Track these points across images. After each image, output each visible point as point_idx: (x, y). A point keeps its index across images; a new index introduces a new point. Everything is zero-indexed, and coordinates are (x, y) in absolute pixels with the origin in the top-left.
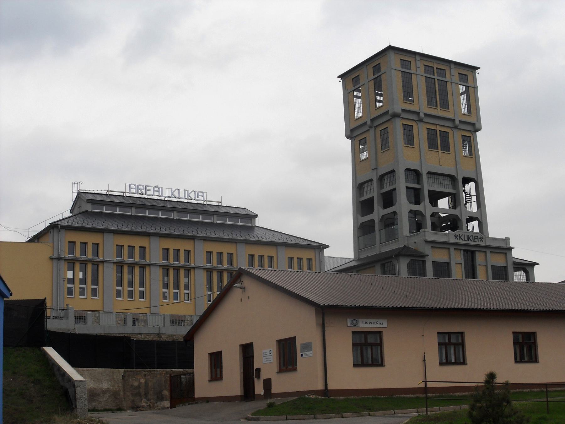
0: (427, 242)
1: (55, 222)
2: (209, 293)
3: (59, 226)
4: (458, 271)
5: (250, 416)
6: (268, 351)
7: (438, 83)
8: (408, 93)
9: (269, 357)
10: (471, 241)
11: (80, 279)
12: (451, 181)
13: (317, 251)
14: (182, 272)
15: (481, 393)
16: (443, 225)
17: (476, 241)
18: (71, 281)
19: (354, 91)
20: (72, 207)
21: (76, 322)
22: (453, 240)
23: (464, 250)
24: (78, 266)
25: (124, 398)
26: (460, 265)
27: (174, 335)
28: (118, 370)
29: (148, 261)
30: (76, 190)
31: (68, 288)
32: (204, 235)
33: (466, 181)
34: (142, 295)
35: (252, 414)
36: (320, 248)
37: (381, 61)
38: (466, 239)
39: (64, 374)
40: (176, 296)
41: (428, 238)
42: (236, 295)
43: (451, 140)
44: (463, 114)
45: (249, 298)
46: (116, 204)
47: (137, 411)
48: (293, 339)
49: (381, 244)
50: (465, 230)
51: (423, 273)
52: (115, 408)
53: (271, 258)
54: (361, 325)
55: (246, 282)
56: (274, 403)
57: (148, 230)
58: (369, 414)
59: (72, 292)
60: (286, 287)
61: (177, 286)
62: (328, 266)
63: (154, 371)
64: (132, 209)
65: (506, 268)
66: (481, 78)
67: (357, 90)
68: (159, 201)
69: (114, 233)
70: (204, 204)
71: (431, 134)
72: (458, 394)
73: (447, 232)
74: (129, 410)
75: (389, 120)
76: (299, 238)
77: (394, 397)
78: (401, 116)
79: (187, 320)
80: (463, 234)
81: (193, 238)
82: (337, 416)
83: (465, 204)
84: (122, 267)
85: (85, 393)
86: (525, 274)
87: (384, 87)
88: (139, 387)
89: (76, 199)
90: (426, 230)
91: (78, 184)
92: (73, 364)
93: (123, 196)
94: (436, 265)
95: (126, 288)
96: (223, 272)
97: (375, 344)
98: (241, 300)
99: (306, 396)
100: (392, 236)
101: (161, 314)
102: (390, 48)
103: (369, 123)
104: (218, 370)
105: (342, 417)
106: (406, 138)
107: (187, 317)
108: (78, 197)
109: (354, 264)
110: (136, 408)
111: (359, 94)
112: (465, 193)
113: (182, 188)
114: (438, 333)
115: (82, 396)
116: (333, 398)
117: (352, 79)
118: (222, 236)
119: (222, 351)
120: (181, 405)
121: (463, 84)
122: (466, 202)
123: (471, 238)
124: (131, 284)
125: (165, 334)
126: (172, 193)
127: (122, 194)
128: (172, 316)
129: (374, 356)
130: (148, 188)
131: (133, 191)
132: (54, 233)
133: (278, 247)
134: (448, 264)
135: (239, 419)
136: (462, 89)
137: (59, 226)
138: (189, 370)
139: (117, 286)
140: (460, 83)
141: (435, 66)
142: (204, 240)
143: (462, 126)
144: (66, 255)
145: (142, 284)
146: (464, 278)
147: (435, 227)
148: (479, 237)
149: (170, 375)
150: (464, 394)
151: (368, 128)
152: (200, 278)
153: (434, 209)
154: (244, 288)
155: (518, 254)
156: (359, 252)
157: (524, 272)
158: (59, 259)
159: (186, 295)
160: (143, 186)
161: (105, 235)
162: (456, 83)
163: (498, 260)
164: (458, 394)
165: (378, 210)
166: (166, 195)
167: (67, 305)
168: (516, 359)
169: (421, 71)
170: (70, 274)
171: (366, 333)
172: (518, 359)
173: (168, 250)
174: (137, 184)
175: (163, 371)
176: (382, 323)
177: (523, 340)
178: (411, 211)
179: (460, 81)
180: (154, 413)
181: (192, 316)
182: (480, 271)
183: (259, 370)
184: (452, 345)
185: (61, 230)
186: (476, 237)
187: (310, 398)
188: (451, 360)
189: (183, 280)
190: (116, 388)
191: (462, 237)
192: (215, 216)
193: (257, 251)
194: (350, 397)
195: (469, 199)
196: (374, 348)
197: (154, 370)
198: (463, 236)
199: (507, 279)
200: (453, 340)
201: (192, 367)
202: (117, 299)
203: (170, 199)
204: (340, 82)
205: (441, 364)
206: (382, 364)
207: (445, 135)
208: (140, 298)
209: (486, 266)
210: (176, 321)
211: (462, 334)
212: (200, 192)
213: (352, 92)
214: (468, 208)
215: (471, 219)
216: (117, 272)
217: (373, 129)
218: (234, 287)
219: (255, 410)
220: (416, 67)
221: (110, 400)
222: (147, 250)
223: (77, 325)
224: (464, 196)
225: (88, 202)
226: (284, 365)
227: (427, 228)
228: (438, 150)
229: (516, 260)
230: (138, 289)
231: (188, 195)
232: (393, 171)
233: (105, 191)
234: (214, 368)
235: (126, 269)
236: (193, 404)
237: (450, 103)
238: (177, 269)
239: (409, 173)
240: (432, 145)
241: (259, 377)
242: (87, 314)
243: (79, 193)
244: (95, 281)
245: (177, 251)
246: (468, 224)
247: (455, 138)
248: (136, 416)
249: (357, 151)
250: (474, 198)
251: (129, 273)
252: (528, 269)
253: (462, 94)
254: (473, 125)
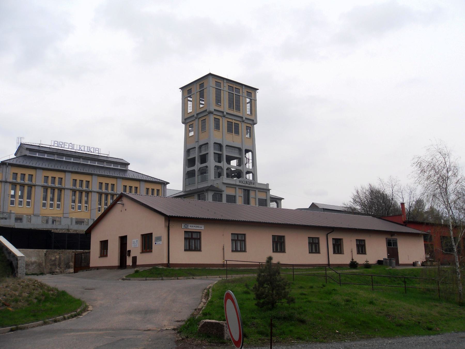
0: (224, 183)
1: (4, 161)
2: (100, 206)
3: (7, 164)
4: (240, 200)
5: (125, 278)
6: (135, 240)
7: (235, 96)
8: (218, 100)
9: (136, 244)
10: (248, 184)
11: (19, 195)
12: (239, 151)
13: (163, 185)
14: (84, 194)
15: (264, 268)
16: (233, 175)
17: (250, 185)
18: (13, 196)
19: (188, 97)
20: (16, 152)
21: (15, 221)
22: (238, 183)
23: (244, 189)
24: (18, 187)
25: (45, 267)
26: (241, 197)
27: (78, 230)
28: (43, 251)
29: (63, 186)
30: (19, 142)
31: (11, 200)
32: (98, 173)
33: (247, 151)
34: (28, 204)
35: (126, 277)
36: (165, 184)
37: (205, 81)
38: (245, 183)
39: (10, 252)
40: (80, 208)
41: (224, 182)
42: (118, 207)
43: (240, 128)
44: (248, 114)
45: (126, 210)
46: (45, 152)
47: (53, 274)
48: (151, 234)
49: (198, 183)
50: (245, 178)
51: (220, 200)
52: (39, 273)
53: (136, 188)
54: (189, 228)
55: (125, 200)
56: (139, 271)
57: (65, 169)
58: (193, 278)
59: (14, 203)
60: (148, 204)
61: (80, 202)
62: (168, 194)
63: (65, 251)
65: (266, 200)
66: (259, 95)
67: (190, 97)
68: (72, 152)
69: (43, 170)
70: (98, 155)
71: (230, 124)
72: (241, 268)
73: (235, 179)
74: (48, 274)
75: (207, 115)
76: (153, 178)
77: (206, 269)
78: (213, 113)
79: (86, 222)
80: (244, 180)
81: (91, 175)
82: (175, 278)
83: (246, 164)
84: (54, 190)
85: (24, 264)
86: (276, 204)
87: (205, 96)
88: (55, 260)
89: (19, 147)
90: (224, 177)
91: (21, 138)
92: (17, 247)
93: (50, 148)
94: (228, 196)
95: (49, 202)
96: (114, 195)
97: (242, 240)
98: (121, 211)
99: (157, 267)
100: (204, 180)
101: (70, 217)
102: (210, 74)
103: (195, 115)
104: (105, 251)
105: (178, 279)
106: (215, 125)
107: (86, 220)
108: (21, 146)
109: (182, 194)
110: (52, 273)
111: (191, 99)
112: (246, 158)
113: (86, 145)
114: (232, 234)
115: (21, 264)
116: (172, 268)
117: (188, 90)
118: (109, 174)
119: (108, 240)
120: (81, 271)
121: (248, 97)
122: (246, 163)
123: (248, 183)
124: (52, 199)
125: (72, 229)
126: (80, 148)
127: (49, 147)
128: (76, 219)
129: (196, 246)
130: (65, 144)
131: (56, 145)
132: (3, 168)
133: (37, 170)
134: (235, 196)
135: (118, 280)
136: (248, 100)
137: (7, 164)
138: (87, 251)
139: (43, 200)
140: (247, 97)
141: (234, 86)
142: (98, 176)
143: (246, 121)
144: (11, 179)
145: (59, 200)
146: (243, 204)
147: (228, 176)
149: (75, 253)
150: (244, 268)
151: (195, 119)
152: (94, 198)
153: (228, 166)
154: (123, 204)
155: (273, 192)
156: (185, 187)
157: (276, 202)
158: (6, 182)
159: (86, 207)
160: (62, 143)
161: (118, 180)
162: (245, 97)
163: (262, 196)
164: (241, 268)
165: (198, 165)
166: (76, 149)
167: (11, 211)
168: (273, 250)
169: (226, 89)
170: (12, 192)
171: (192, 232)
172: (275, 250)
173: (76, 180)
174: (59, 141)
175: (71, 251)
176: (201, 227)
177: (277, 240)
178: (216, 166)
179: (247, 96)
180: (64, 276)
181: (88, 219)
182: (252, 201)
183: (129, 251)
184: (239, 241)
185: (8, 166)
186: (251, 182)
187: (160, 268)
188: (238, 249)
189: (84, 198)
190: (41, 261)
191: (243, 182)
192: (105, 163)
193: (128, 184)
194: (198, 268)
195: (248, 161)
196: (241, 242)
197: (65, 250)
199: (266, 206)
200: (240, 238)
201: (89, 249)
202: (43, 208)
203: (78, 151)
204: (180, 91)
205: (233, 251)
206: (200, 250)
207: (237, 126)
208: (57, 208)
209: (255, 198)
210: (79, 222)
211: (245, 235)
212: (97, 148)
213: (187, 98)
214: (247, 167)
215: (248, 172)
216: (44, 192)
217: (198, 119)
218: (118, 203)
219: (128, 274)
220: (243, 92)
221: (36, 268)
222: (90, 183)
223: (16, 223)
224: (245, 159)
225: (27, 150)
226: (145, 249)
227: (224, 176)
228: (232, 133)
229: (271, 196)
230: (56, 202)
231: (90, 150)
232: (207, 143)
233: (38, 144)
234: (103, 250)
235: (49, 191)
236: (88, 270)
237: (241, 108)
238: (81, 192)
239: (216, 145)
240: (230, 130)
241: (129, 255)
242: (23, 217)
243: (21, 144)
244: (29, 197)
245: (82, 181)
246: (247, 175)
247: (242, 127)
248: (54, 278)
249: (188, 131)
250: (251, 161)
251: (85, 197)
252: (278, 201)
253: (248, 103)
254: (253, 120)
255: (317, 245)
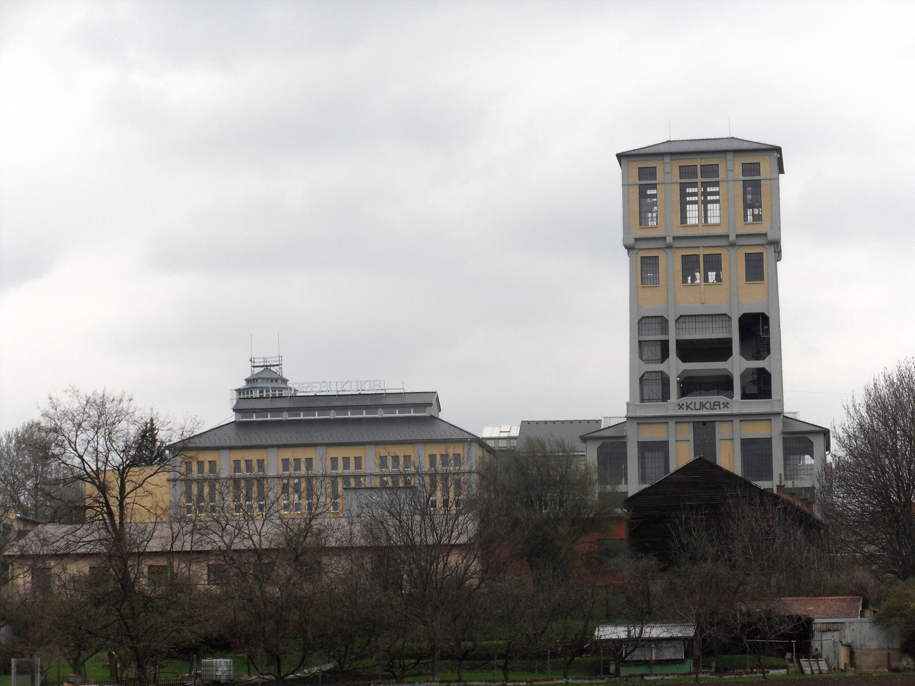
64: (44, 425)
68: (366, 396)
130: (314, 385)
148: (721, 403)
198: (693, 405)
255: (760, 217)
